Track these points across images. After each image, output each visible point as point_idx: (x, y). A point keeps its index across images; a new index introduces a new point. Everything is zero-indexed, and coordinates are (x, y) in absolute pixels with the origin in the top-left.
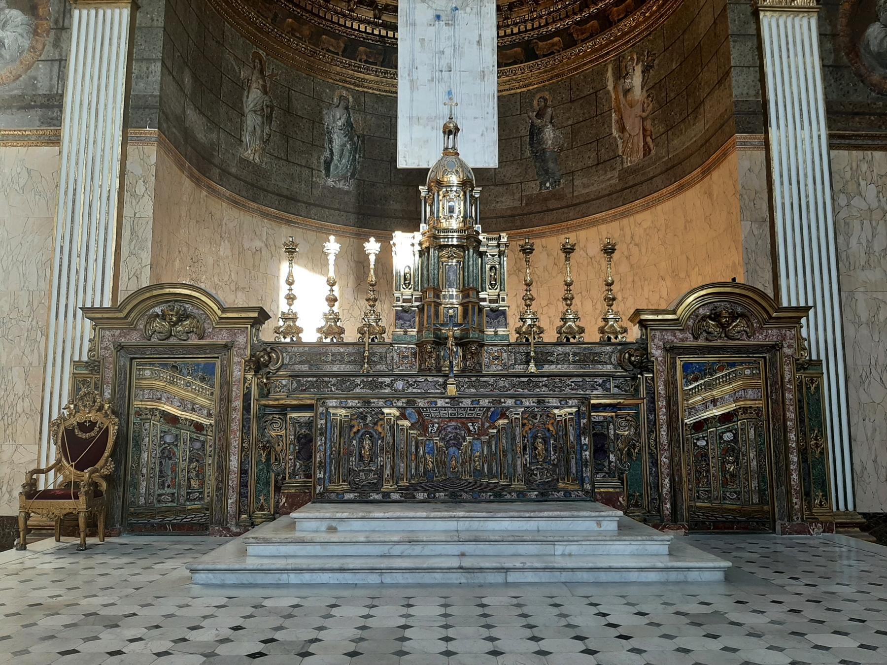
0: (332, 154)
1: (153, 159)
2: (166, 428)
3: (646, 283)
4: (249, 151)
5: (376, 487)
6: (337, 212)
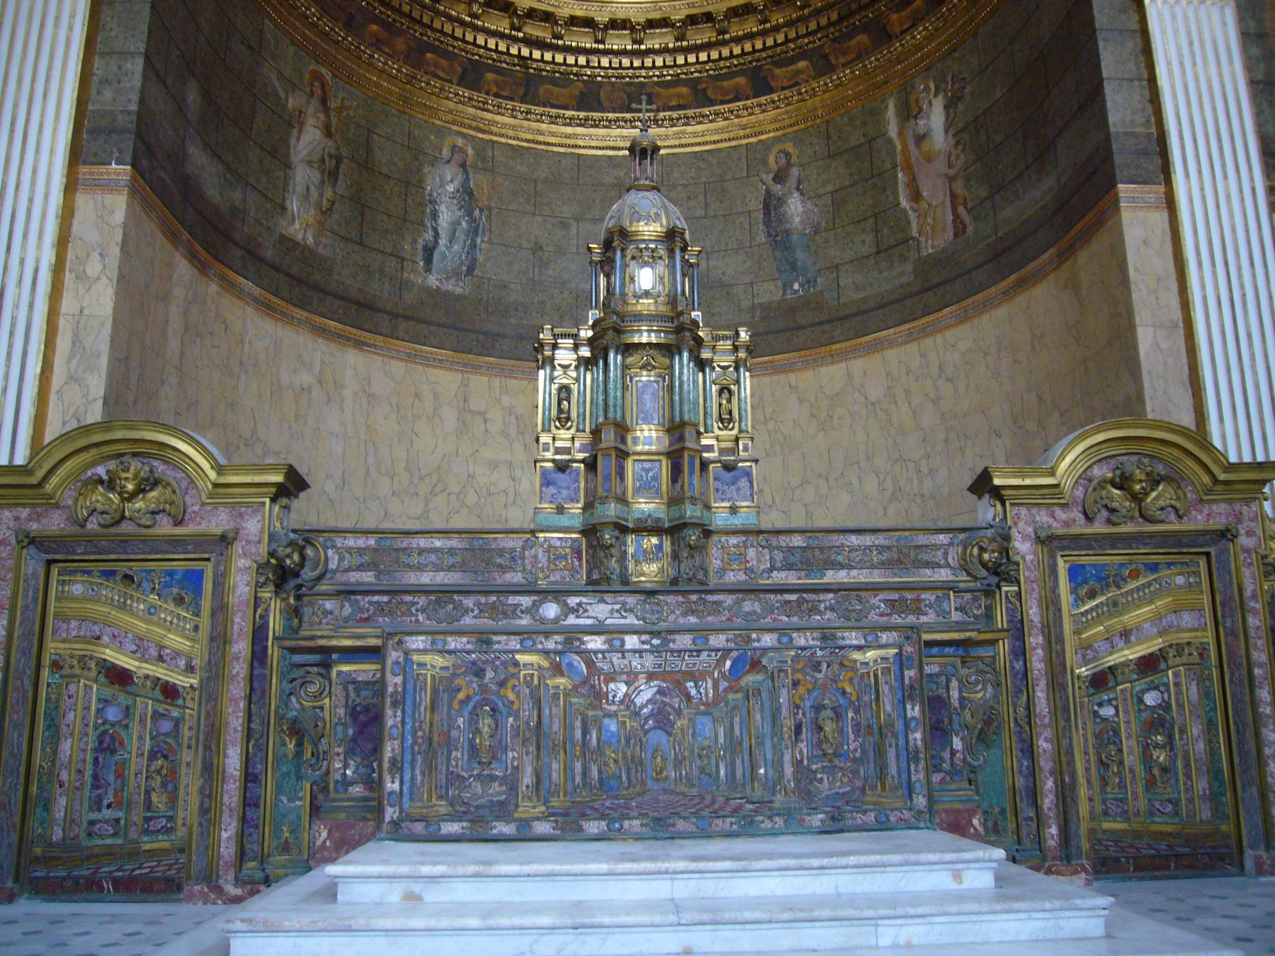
0: (437, 235)
1: (119, 216)
2: (108, 692)
3: (969, 442)
4: (297, 225)
5: (503, 810)
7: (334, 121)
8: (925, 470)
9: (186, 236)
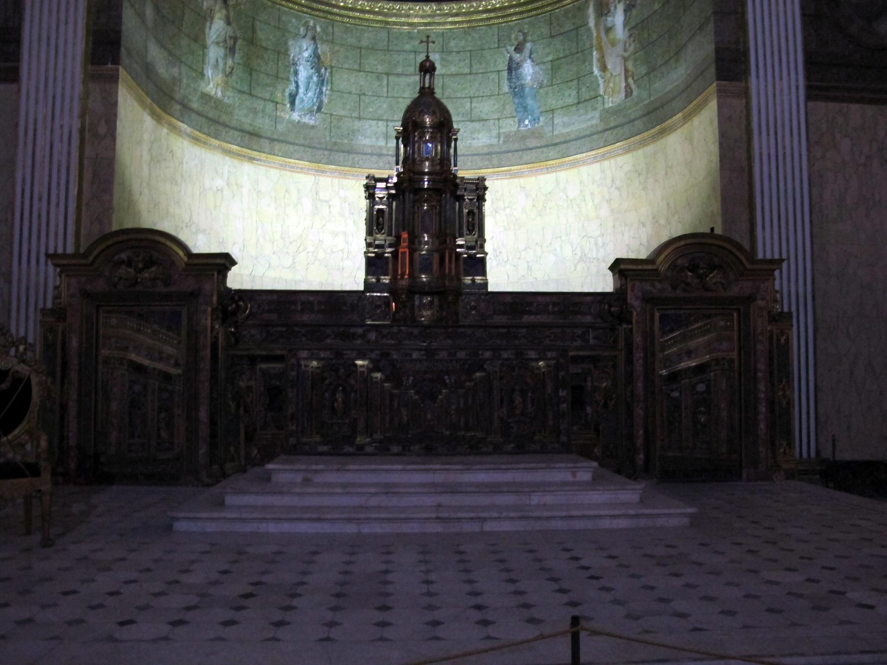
0: (297, 87)
4: (211, 85)
6: (302, 148)
7: (232, 14)
8: (600, 243)
9: (149, 101)
